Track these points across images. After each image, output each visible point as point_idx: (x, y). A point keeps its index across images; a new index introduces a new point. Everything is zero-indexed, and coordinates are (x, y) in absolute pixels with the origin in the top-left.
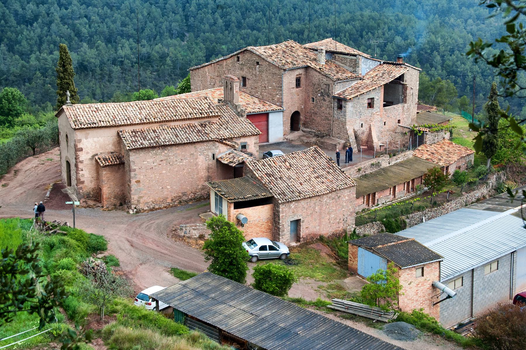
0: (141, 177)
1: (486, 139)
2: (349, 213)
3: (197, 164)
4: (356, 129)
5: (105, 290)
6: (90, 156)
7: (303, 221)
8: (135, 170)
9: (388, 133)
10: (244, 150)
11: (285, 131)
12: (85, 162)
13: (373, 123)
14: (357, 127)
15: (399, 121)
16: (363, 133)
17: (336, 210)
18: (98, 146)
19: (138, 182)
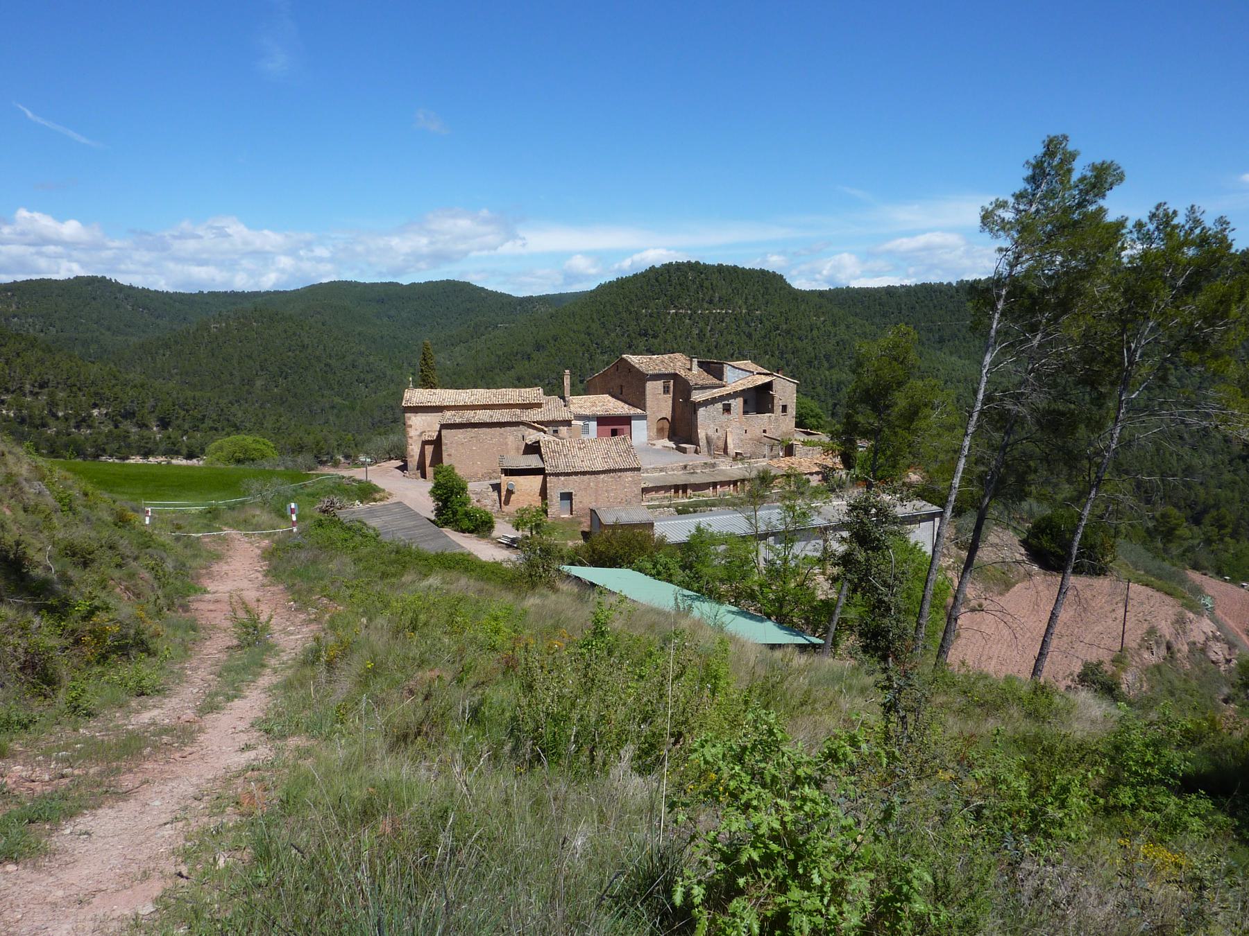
0: (452, 451)
1: (824, 438)
2: (633, 495)
3: (506, 444)
4: (709, 433)
5: (785, 742)
6: (418, 433)
7: (575, 495)
8: (446, 444)
9: (751, 442)
10: (556, 434)
11: (649, 436)
12: (414, 438)
13: (730, 429)
14: (711, 433)
15: (765, 431)
16: (719, 438)
17: (616, 489)
18: (426, 424)
19: (449, 455)
